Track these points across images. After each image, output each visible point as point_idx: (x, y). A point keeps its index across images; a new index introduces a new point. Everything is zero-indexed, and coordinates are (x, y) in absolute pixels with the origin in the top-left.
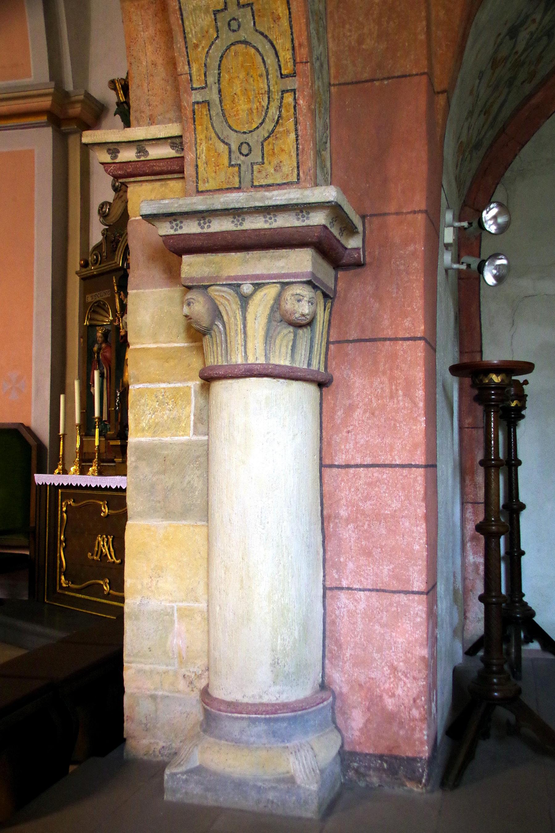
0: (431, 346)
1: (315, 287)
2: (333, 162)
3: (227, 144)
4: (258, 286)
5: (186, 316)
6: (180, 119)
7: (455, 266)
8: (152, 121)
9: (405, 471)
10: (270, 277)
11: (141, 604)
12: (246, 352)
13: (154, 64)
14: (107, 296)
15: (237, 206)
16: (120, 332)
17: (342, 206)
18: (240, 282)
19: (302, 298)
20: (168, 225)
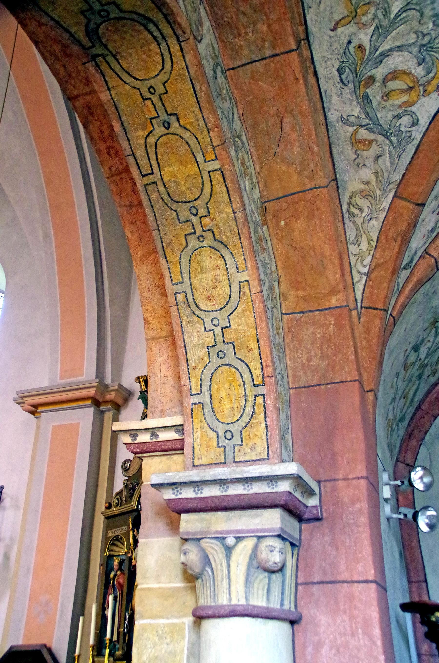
0: (380, 585)
1: (284, 539)
2: (294, 441)
3: (215, 431)
4: (239, 539)
5: (183, 563)
6: (182, 413)
7: (395, 516)
8: (163, 414)
10: (248, 531)
12: (230, 594)
13: (166, 377)
14: (124, 531)
16: (132, 562)
17: (302, 476)
18: (225, 536)
19: (273, 549)
20: (170, 491)
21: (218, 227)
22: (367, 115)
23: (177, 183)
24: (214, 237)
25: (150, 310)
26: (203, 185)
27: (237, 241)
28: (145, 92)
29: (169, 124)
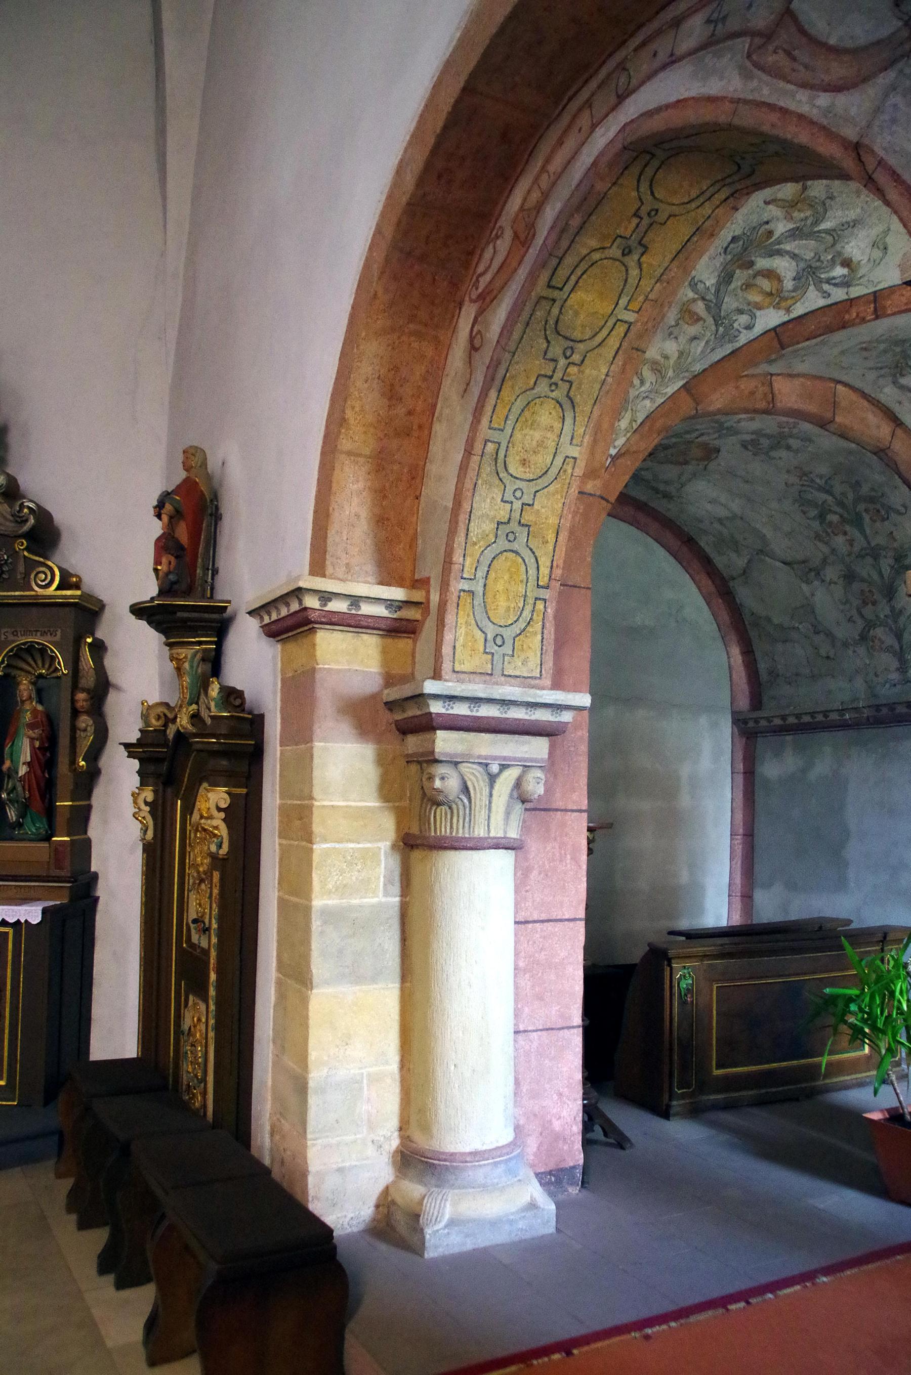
3: (484, 632)
4: (503, 767)
9: (571, 924)
10: (515, 759)
11: (327, 1077)
13: (357, 516)
15: (513, 699)
21: (580, 384)
22: (718, 291)
23: (577, 313)
24: (569, 392)
25: (357, 409)
26: (601, 330)
27: (588, 409)
28: (644, 210)
29: (630, 252)
